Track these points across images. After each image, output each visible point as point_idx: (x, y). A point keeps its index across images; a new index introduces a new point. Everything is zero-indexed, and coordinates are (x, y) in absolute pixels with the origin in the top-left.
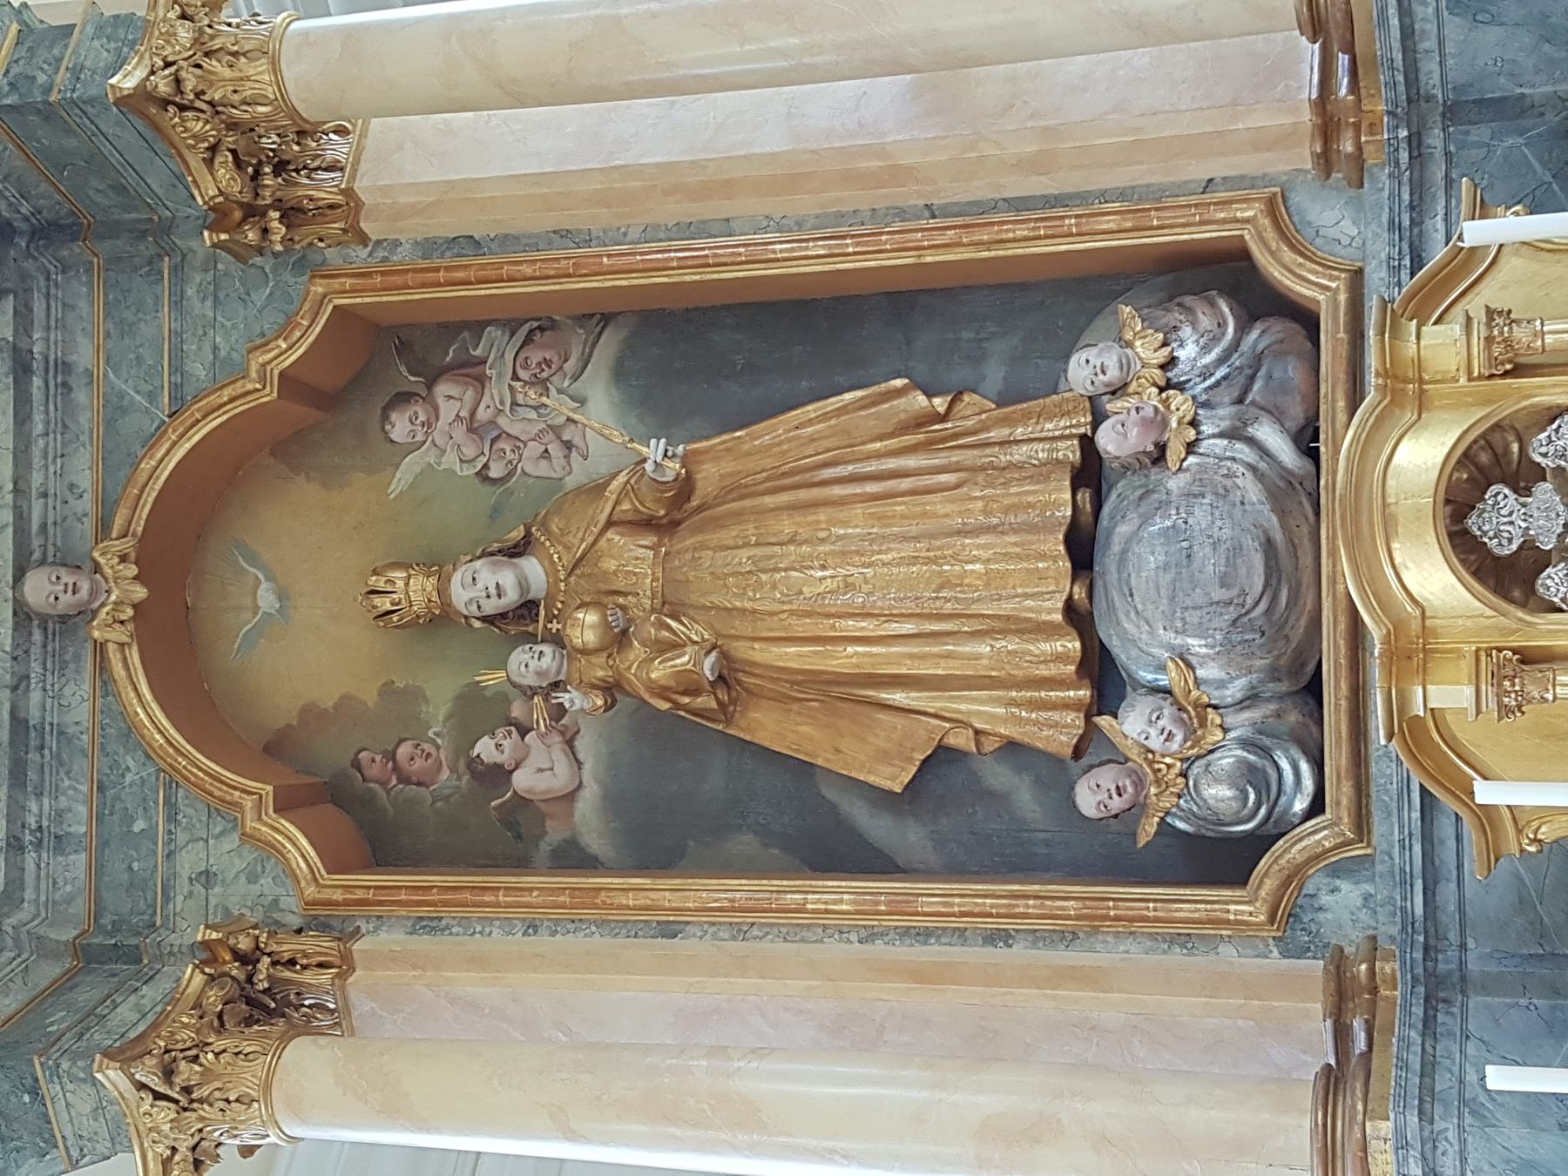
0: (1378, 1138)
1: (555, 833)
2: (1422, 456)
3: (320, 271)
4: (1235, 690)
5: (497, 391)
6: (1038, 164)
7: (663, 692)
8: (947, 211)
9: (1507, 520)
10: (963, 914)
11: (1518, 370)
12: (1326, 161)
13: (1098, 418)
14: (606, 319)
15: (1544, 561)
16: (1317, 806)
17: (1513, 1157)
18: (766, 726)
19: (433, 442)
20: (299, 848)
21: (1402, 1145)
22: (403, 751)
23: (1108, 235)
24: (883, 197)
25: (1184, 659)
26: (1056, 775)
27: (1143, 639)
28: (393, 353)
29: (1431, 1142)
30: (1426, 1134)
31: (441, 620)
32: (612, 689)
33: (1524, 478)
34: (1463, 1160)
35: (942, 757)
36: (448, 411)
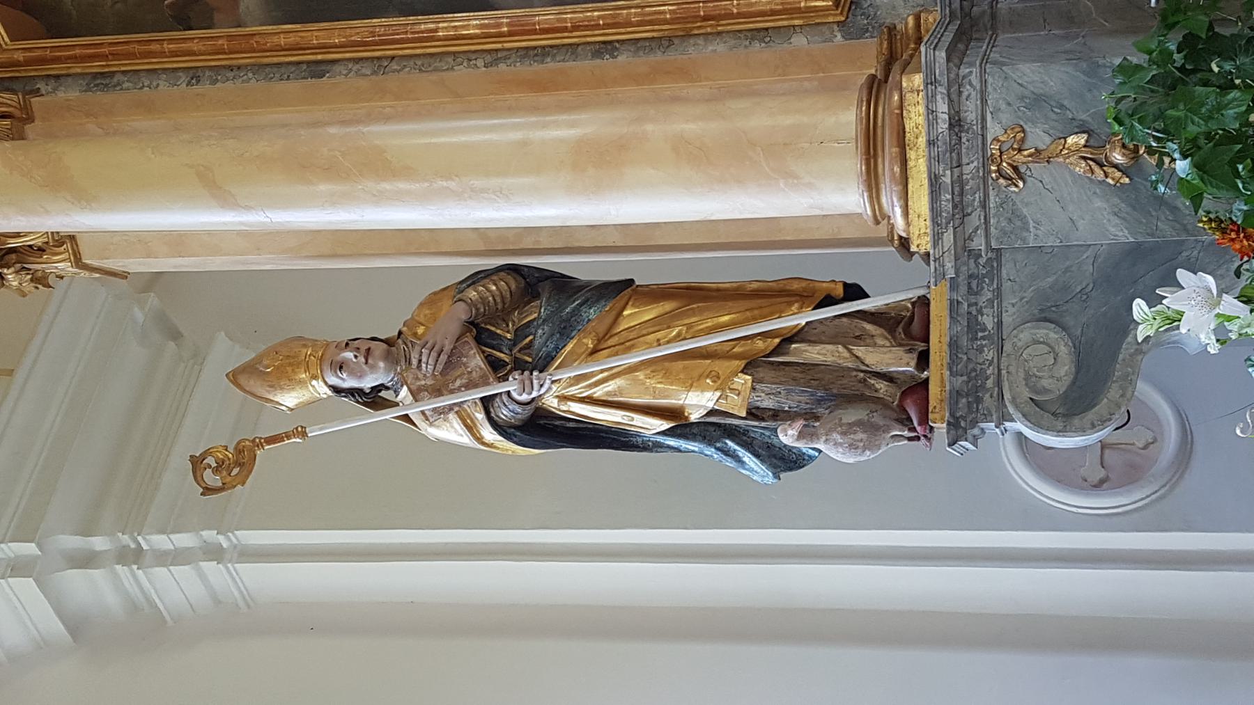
0: (912, 92)
10: (576, 28)
17: (1027, 93)
21: (931, 82)
30: (952, 76)
34: (984, 101)
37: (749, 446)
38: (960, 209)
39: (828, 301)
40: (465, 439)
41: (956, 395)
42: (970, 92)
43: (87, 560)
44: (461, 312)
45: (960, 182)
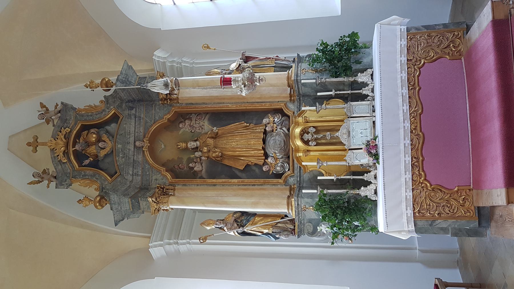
1: (199, 175)
2: (298, 130)
3: (173, 106)
4: (280, 157)
5: (193, 122)
6: (260, 98)
7: (214, 157)
8: (249, 103)
9: (306, 137)
11: (307, 122)
12: (291, 100)
13: (266, 127)
14: (207, 113)
15: (310, 141)
16: (289, 170)
18: (226, 162)
19: (185, 128)
20: (169, 176)
21: (295, 200)
22: (180, 165)
23: (267, 106)
24: (242, 101)
25: (275, 153)
26: (260, 167)
27: (270, 151)
28: (182, 116)
29: (298, 200)
31: (187, 149)
32: (208, 157)
33: (308, 133)
35: (248, 166)
36: (187, 124)
37: (272, 236)
38: (299, 214)
39: (282, 218)
40: (233, 234)
41: (299, 232)
42: (300, 201)
43: (170, 244)
44: (234, 218)
45: (298, 211)
